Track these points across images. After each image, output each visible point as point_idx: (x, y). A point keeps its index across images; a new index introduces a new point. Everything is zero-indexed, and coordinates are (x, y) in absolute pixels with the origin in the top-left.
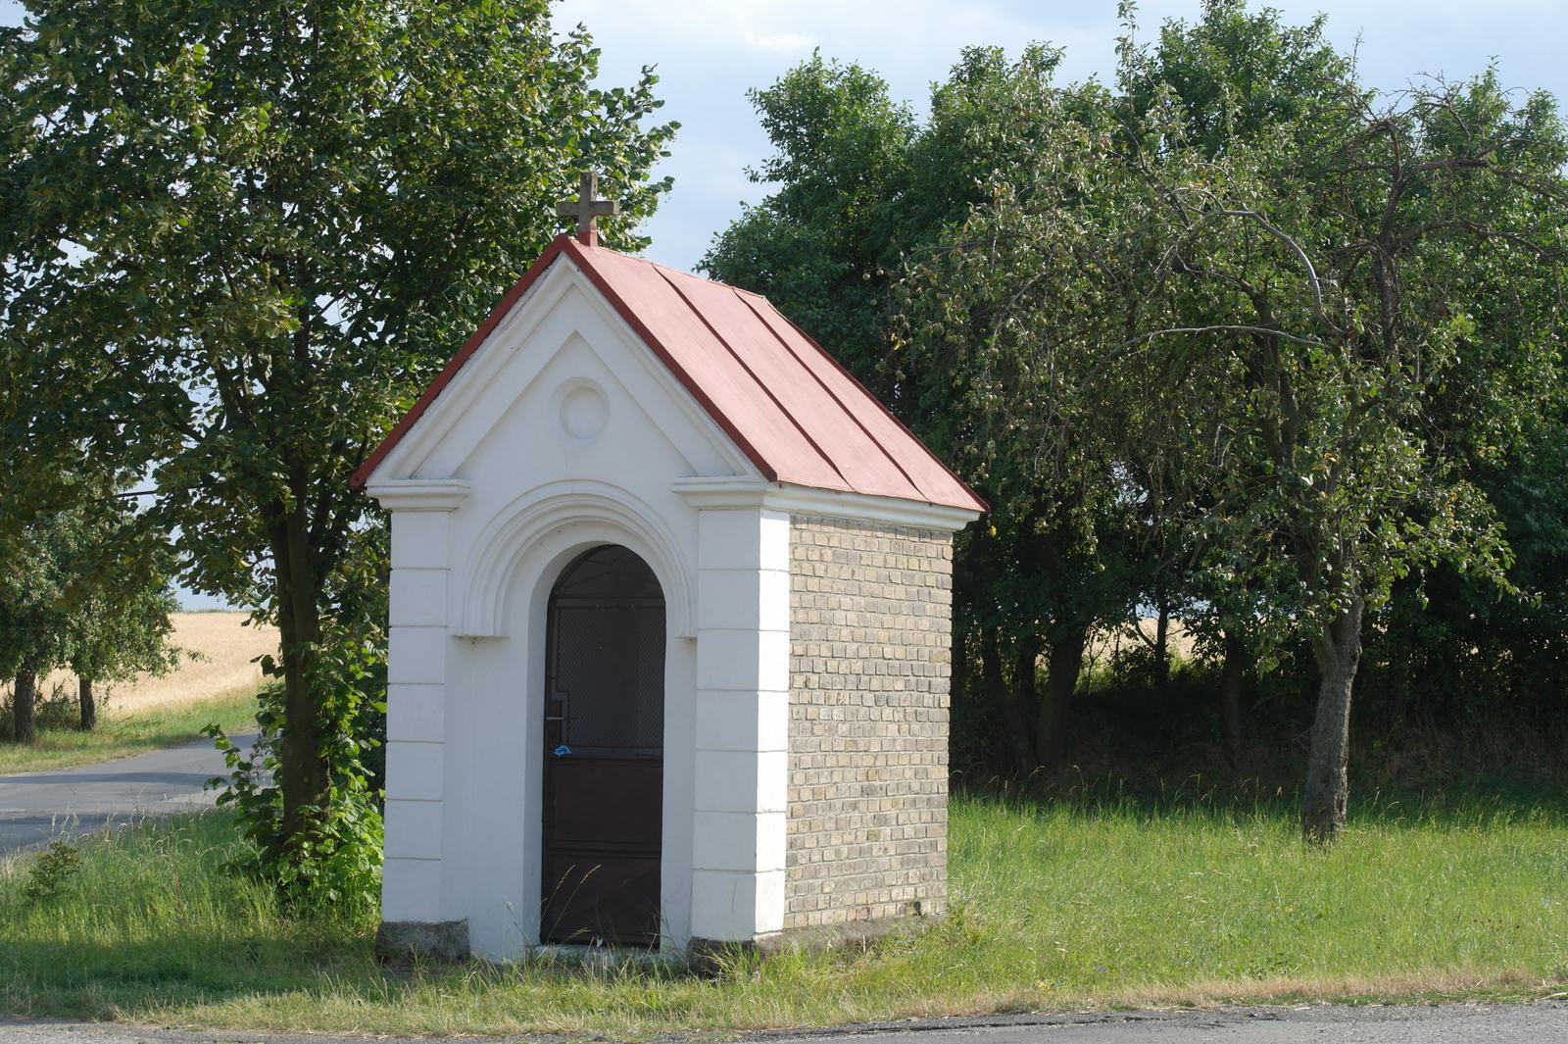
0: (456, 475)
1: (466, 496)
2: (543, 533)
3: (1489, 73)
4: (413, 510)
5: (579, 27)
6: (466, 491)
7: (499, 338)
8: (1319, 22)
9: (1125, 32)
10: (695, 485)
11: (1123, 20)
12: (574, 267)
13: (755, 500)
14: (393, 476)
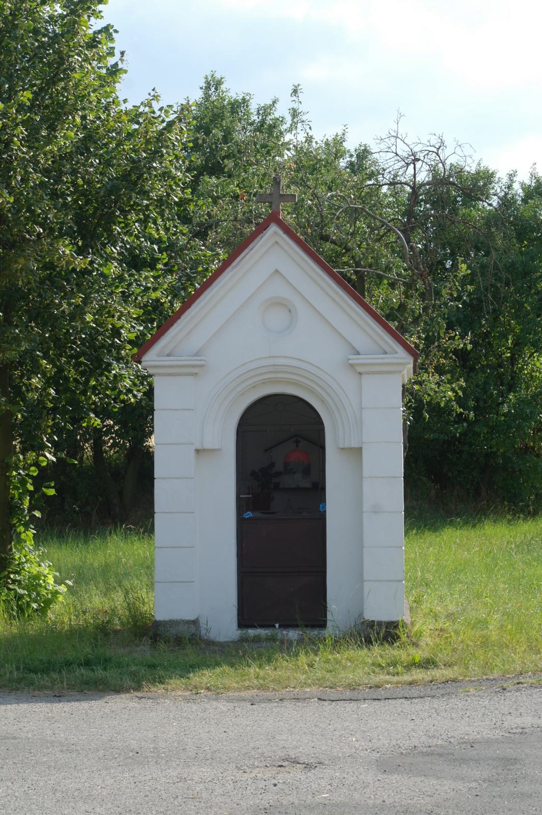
0: (197, 354)
1: (202, 366)
2: (303, 384)
3: (344, 134)
4: (169, 375)
5: (153, 90)
6: (203, 362)
7: (231, 274)
8: (274, 102)
9: (295, 106)
10: (355, 359)
11: (294, 98)
12: (281, 232)
13: (196, 370)
14: (158, 355)
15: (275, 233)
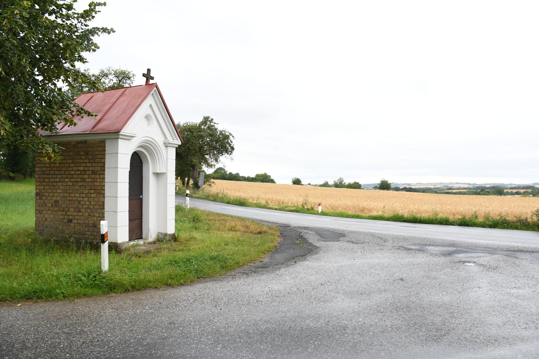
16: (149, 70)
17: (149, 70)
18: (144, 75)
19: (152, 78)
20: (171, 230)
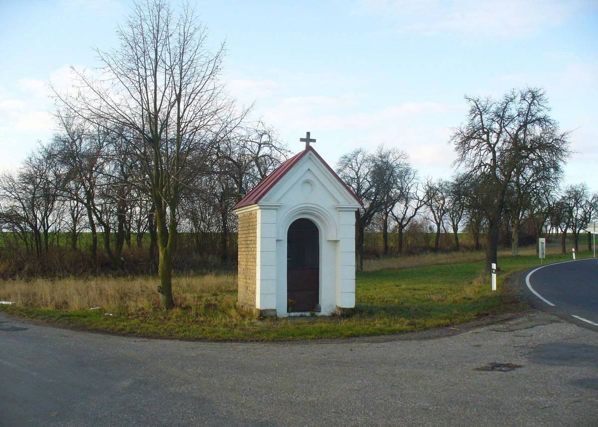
15: (310, 154)
16: (308, 134)
17: (308, 134)
18: (302, 140)
19: (314, 141)
20: (349, 302)
